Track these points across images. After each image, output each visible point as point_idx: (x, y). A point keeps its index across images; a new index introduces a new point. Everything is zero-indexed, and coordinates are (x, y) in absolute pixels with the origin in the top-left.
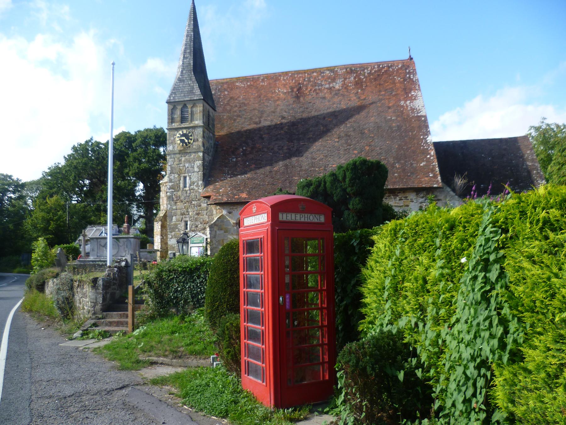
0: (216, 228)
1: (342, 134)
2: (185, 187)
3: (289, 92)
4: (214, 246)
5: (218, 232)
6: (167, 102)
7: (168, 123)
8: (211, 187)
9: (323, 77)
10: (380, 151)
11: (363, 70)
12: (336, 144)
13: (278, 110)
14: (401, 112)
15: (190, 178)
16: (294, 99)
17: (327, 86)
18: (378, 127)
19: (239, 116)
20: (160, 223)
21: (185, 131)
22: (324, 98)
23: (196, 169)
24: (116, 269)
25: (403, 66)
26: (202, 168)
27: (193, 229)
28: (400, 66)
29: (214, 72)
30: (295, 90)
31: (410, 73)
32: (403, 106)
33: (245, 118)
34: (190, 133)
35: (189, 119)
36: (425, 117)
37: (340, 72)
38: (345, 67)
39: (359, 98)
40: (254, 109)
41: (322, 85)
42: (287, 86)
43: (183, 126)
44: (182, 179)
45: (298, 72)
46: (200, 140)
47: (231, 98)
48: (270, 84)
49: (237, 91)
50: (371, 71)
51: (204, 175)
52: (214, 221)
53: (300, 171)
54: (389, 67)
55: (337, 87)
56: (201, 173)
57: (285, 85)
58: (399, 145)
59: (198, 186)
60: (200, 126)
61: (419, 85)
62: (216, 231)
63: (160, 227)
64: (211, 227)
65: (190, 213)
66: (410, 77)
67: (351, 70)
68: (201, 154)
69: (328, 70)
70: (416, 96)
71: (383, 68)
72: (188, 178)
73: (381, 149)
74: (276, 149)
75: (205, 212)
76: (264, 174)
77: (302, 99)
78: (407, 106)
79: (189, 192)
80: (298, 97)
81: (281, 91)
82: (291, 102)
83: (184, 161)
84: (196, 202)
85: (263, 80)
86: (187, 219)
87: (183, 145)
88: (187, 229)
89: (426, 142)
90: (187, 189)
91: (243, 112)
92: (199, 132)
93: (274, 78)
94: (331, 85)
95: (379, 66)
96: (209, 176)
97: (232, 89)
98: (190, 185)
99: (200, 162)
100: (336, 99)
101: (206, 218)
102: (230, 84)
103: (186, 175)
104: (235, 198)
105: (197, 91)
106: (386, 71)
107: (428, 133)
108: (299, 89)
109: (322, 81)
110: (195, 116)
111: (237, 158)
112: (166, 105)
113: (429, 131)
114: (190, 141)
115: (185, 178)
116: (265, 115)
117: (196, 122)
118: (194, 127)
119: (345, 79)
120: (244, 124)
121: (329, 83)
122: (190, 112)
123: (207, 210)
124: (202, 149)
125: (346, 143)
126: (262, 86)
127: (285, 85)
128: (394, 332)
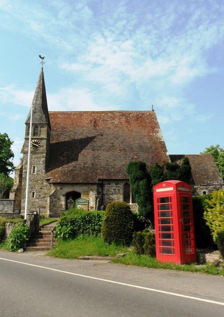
0: (53, 197)
1: (122, 149)
2: (34, 172)
3: (89, 123)
4: (52, 208)
5: (54, 200)
6: (25, 124)
7: (26, 135)
8: (50, 173)
9: (107, 116)
10: (143, 159)
11: (129, 115)
12: (119, 154)
13: (84, 132)
14: (151, 138)
15: (37, 168)
16: (93, 127)
17: (111, 121)
18: (140, 146)
19: (62, 134)
20: (14, 193)
21: (36, 141)
22: (109, 128)
23: (41, 163)
24: (33, 216)
25: (150, 114)
26: (45, 163)
27: (37, 197)
28: (148, 114)
29: (51, 108)
30: (93, 122)
31: (153, 118)
32: (152, 136)
33: (66, 136)
34: (38, 142)
35: (39, 134)
36: (164, 142)
37: (117, 114)
38: (120, 112)
39: (128, 129)
40: (70, 131)
41: (107, 121)
42: (88, 120)
43: (35, 138)
44: (32, 167)
45: (93, 112)
46: (45, 146)
47: (56, 123)
48: (78, 117)
49: (59, 119)
50: (133, 115)
51: (46, 166)
52: (52, 193)
53: (100, 167)
54: (142, 114)
55: (116, 122)
56: (44, 165)
57: (87, 119)
58: (152, 156)
59: (42, 172)
60: (45, 139)
61: (159, 125)
62: (53, 199)
63: (14, 195)
64: (50, 196)
65: (36, 188)
66: (153, 121)
67: (123, 114)
68: (45, 154)
69: (110, 113)
70: (158, 131)
71: (139, 114)
72: (36, 168)
73: (143, 158)
74: (85, 154)
75: (46, 187)
76: (80, 168)
77: (97, 127)
78: (154, 136)
79: (36, 176)
80: (95, 126)
81: (86, 122)
82: (91, 129)
83: (34, 158)
84: (40, 182)
85: (74, 115)
86: (34, 191)
87: (34, 149)
88: (33, 197)
89: (166, 155)
90: (35, 173)
91: (65, 132)
92: (44, 142)
93: (81, 114)
94: (113, 121)
95: (137, 113)
96: (49, 166)
97: (56, 118)
98: (37, 172)
99: (44, 159)
100: (116, 129)
101: (46, 191)
102: (56, 114)
103: (35, 166)
104: (65, 181)
105: (44, 119)
106: (141, 116)
107: (166, 151)
108: (95, 122)
109: (107, 119)
110: (42, 133)
111: (63, 158)
112: (25, 125)
113: (167, 150)
114: (39, 144)
115: (34, 167)
116: (77, 135)
117: (43, 136)
118: (41, 139)
119: (120, 119)
120: (63, 138)
121: (111, 120)
122: (39, 130)
123: (47, 186)
124: (46, 151)
125: (124, 153)
126: (74, 118)
127: (87, 119)
128: (217, 236)
